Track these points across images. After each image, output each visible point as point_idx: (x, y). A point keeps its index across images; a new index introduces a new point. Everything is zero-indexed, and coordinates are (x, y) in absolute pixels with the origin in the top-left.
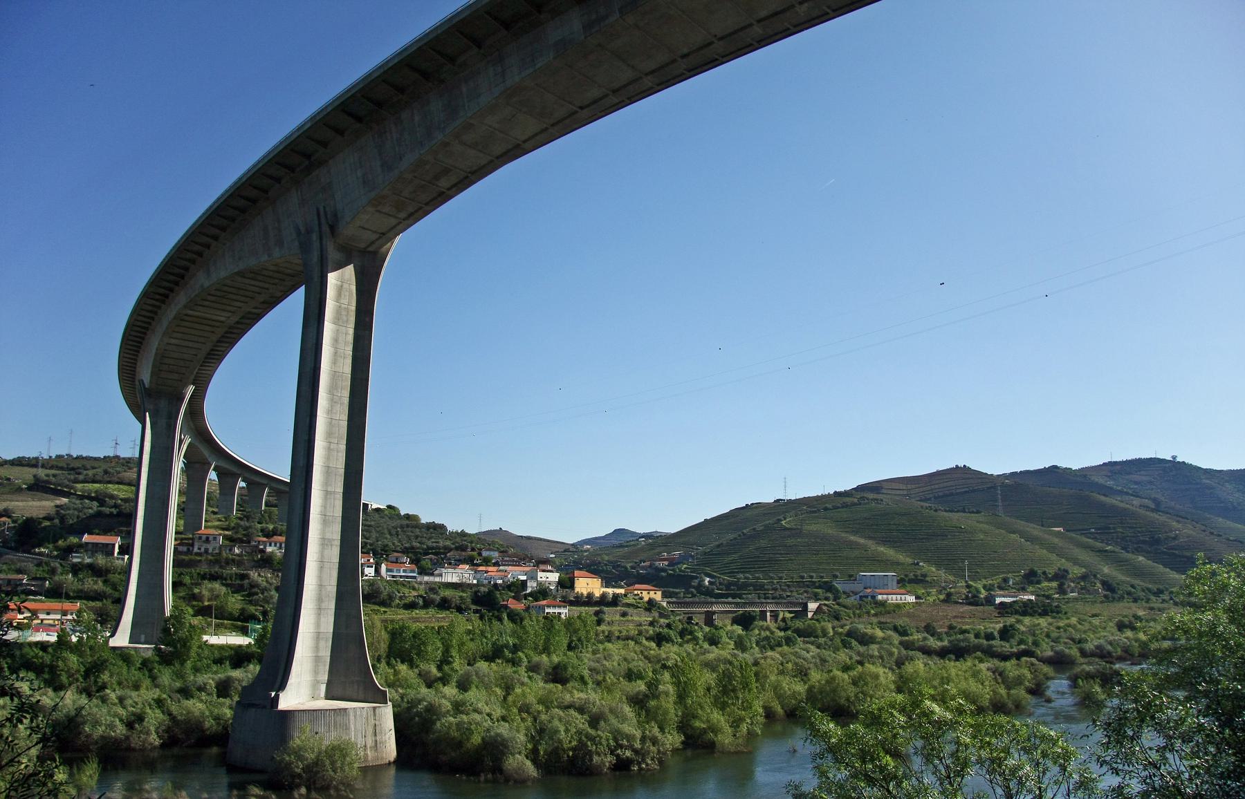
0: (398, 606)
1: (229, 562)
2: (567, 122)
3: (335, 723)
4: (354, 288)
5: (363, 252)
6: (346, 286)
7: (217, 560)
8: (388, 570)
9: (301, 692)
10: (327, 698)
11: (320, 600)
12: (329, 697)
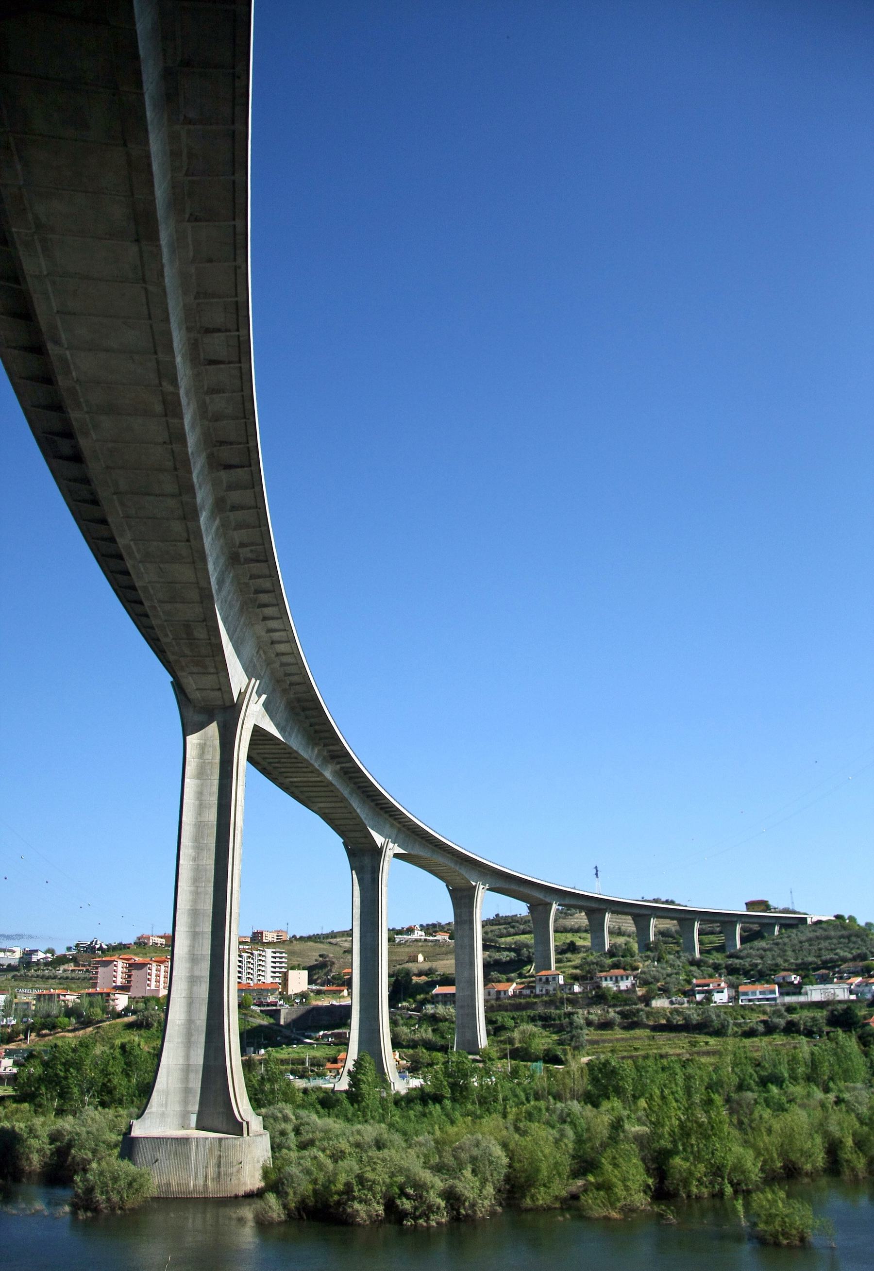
0: (735, 1035)
12: (199, 1127)
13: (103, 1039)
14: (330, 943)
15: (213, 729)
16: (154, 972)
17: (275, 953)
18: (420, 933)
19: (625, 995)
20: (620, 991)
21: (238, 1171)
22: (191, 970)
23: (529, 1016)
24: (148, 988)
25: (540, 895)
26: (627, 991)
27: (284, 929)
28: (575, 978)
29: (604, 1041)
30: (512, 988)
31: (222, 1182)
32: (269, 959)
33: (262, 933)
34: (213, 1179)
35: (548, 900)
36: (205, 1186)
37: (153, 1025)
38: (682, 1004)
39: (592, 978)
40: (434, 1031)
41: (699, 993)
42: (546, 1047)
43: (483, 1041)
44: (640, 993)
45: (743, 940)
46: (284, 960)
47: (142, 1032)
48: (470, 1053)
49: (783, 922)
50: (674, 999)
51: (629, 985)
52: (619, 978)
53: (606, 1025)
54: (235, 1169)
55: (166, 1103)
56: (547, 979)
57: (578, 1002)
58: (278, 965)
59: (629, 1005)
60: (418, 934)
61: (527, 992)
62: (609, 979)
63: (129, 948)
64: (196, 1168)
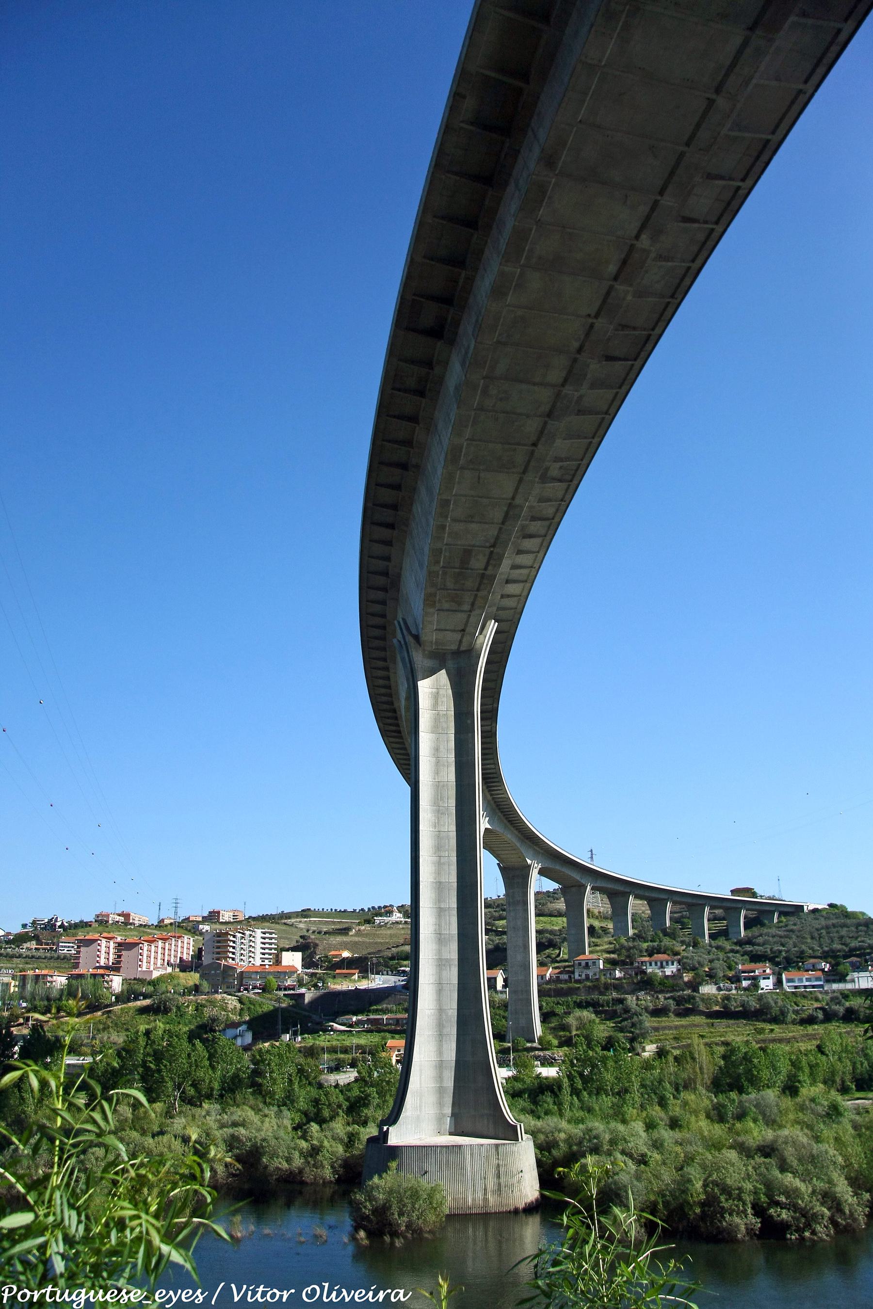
0: (794, 1022)
1: (607, 987)
2: (533, 463)
3: (448, 1161)
4: (450, 692)
5: (457, 653)
6: (442, 692)
7: (597, 987)
8: (789, 981)
9: (421, 1123)
10: (451, 1134)
11: (440, 1026)
13: (116, 1024)
14: (285, 924)
17: (264, 933)
18: (399, 915)
19: (671, 981)
20: (667, 977)
21: (519, 1182)
22: (439, 952)
23: (575, 1002)
24: (140, 969)
25: (576, 876)
26: (673, 976)
27: (242, 909)
28: (614, 963)
29: (664, 1028)
31: (504, 1194)
32: (259, 940)
33: (218, 912)
34: (493, 1192)
35: (583, 881)
36: (486, 1200)
37: (171, 1010)
38: (730, 990)
39: (632, 964)
41: (745, 979)
42: (606, 1034)
44: (686, 979)
45: (746, 927)
46: (273, 941)
47: (160, 1017)
48: (528, 1041)
49: (782, 909)
50: (722, 985)
51: (675, 970)
52: (664, 963)
54: (515, 1179)
55: (421, 1106)
56: (587, 964)
57: (623, 987)
58: (267, 946)
59: (677, 991)
62: (653, 964)
63: (90, 926)
64: (473, 1180)
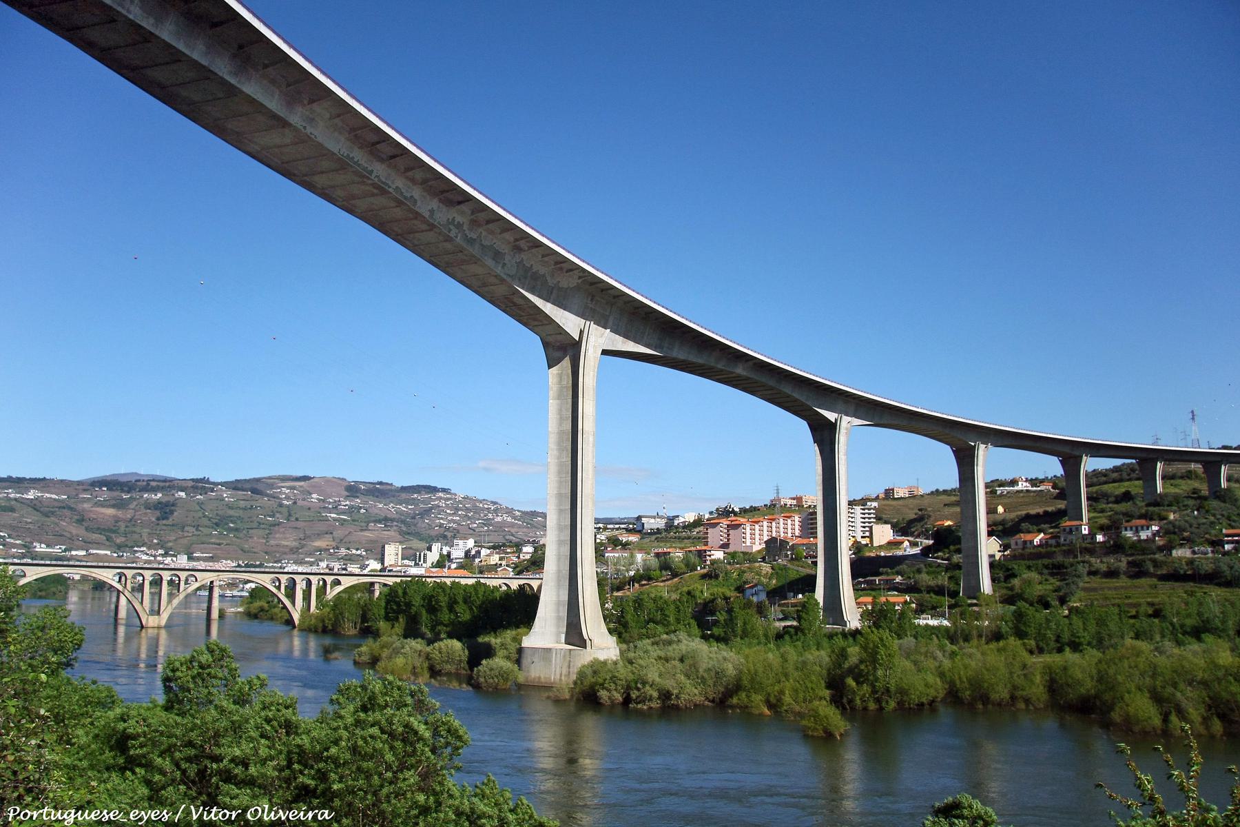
15: (566, 362)
16: (748, 531)
20: (1140, 541)
30: (1038, 539)
40: (950, 578)
43: (986, 585)
53: (1112, 574)
60: (1022, 486)
61: (1053, 542)
